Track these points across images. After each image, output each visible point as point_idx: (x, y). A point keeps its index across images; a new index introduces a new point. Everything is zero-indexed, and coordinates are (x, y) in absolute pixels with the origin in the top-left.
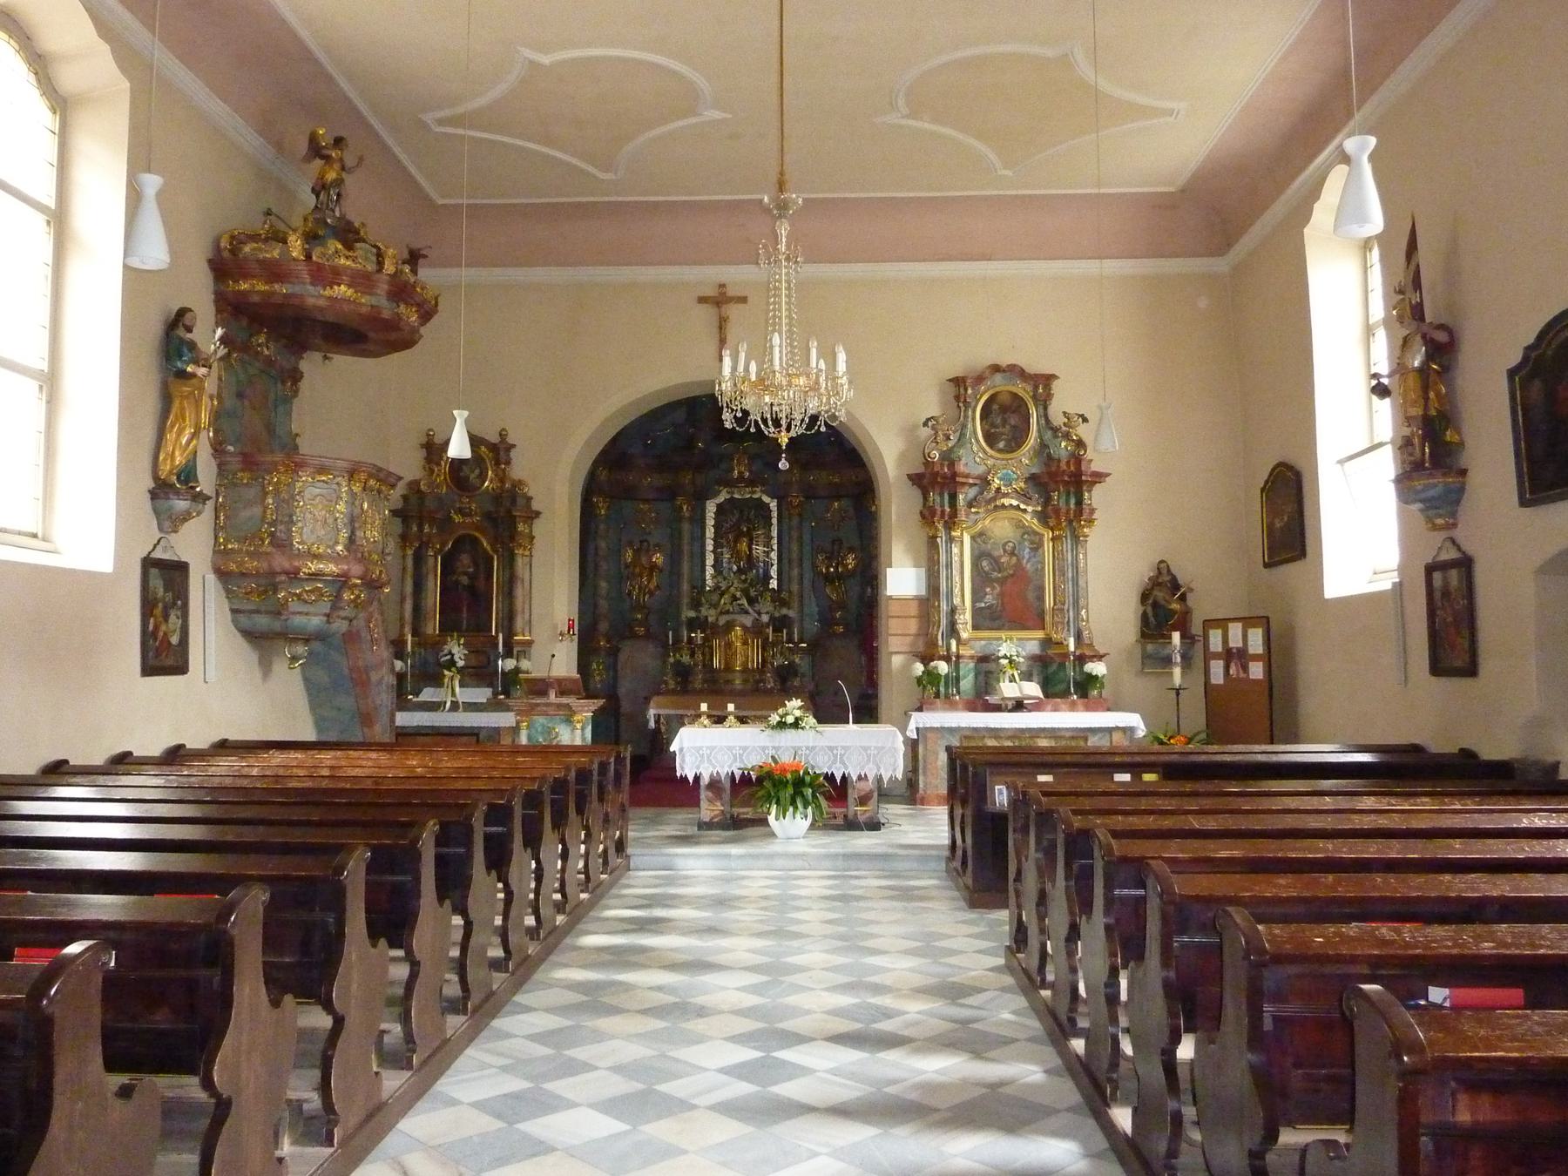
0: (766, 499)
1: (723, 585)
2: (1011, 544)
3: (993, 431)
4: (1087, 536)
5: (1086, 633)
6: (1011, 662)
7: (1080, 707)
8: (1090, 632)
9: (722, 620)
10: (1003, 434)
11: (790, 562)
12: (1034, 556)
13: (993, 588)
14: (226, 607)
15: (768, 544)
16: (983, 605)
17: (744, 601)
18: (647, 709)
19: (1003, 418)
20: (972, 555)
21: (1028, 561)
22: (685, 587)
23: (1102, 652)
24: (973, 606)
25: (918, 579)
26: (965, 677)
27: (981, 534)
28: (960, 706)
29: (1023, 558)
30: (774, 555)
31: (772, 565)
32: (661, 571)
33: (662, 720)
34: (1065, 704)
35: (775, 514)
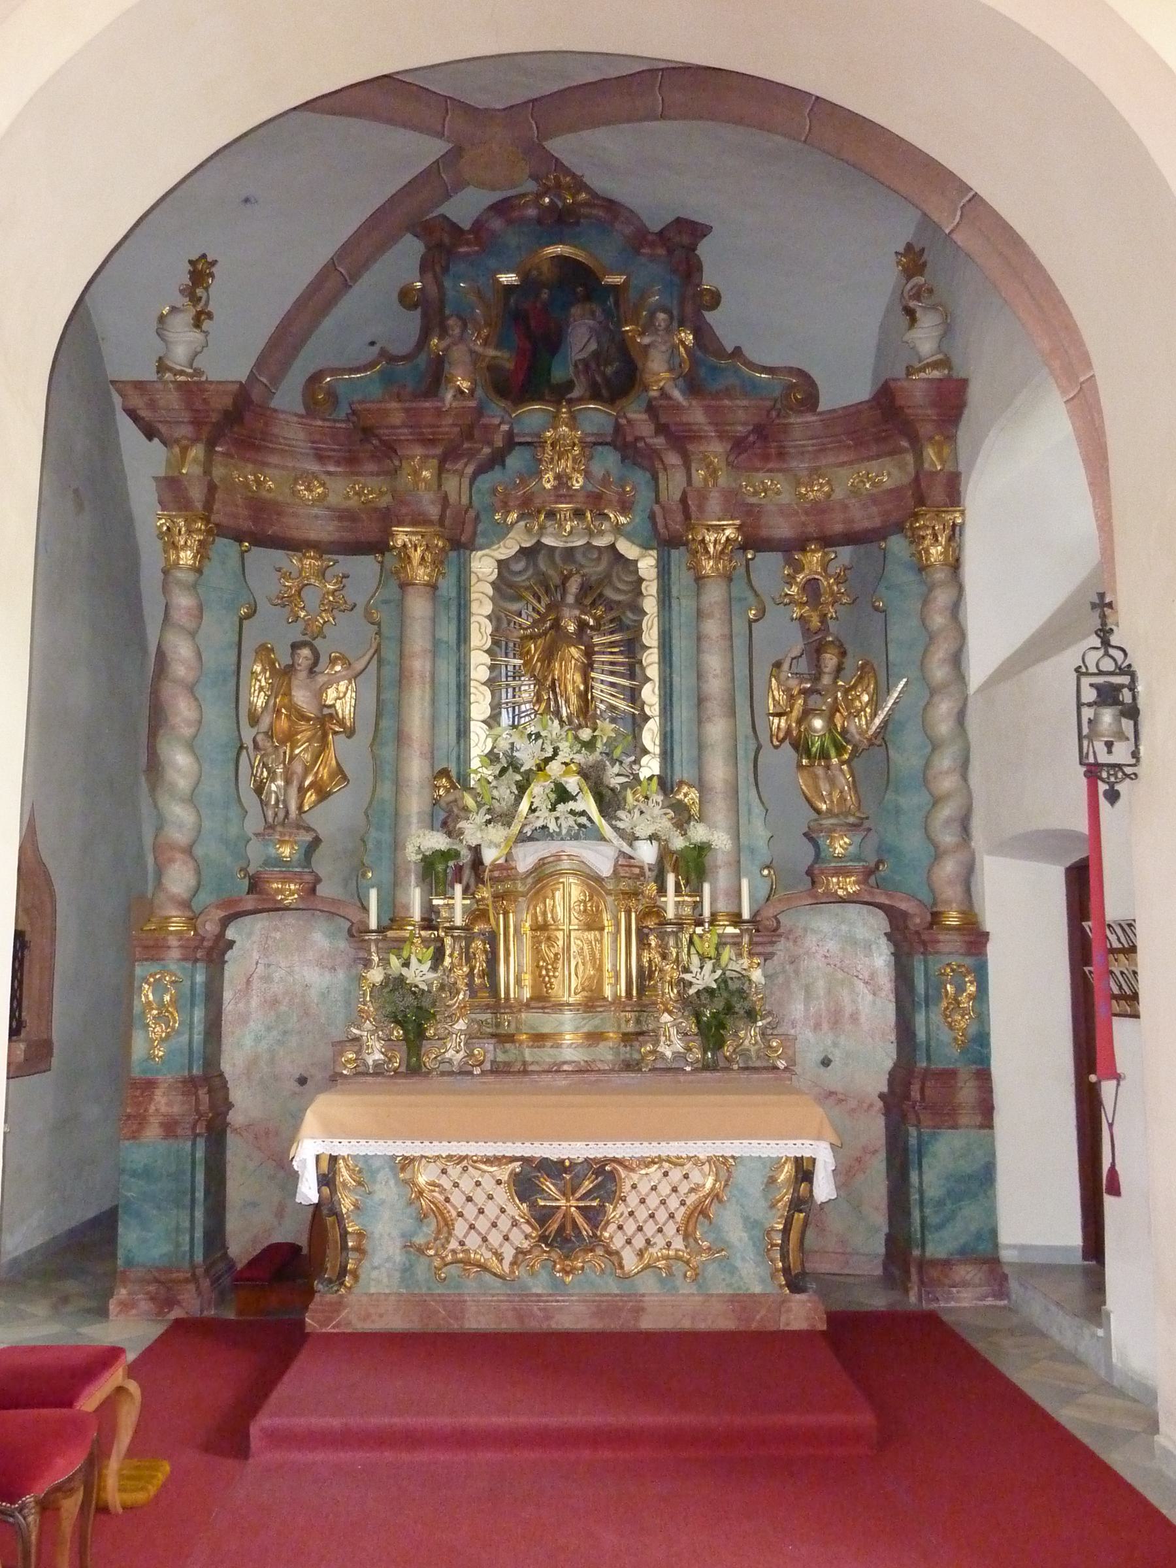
0: (628, 549)
1: (528, 756)
9: (526, 858)
11: (700, 701)
15: (634, 670)
17: (588, 804)
18: (292, 1138)
22: (416, 769)
24: (701, 897)
30: (650, 695)
31: (647, 718)
32: (350, 733)
33: (344, 1175)
35: (651, 589)
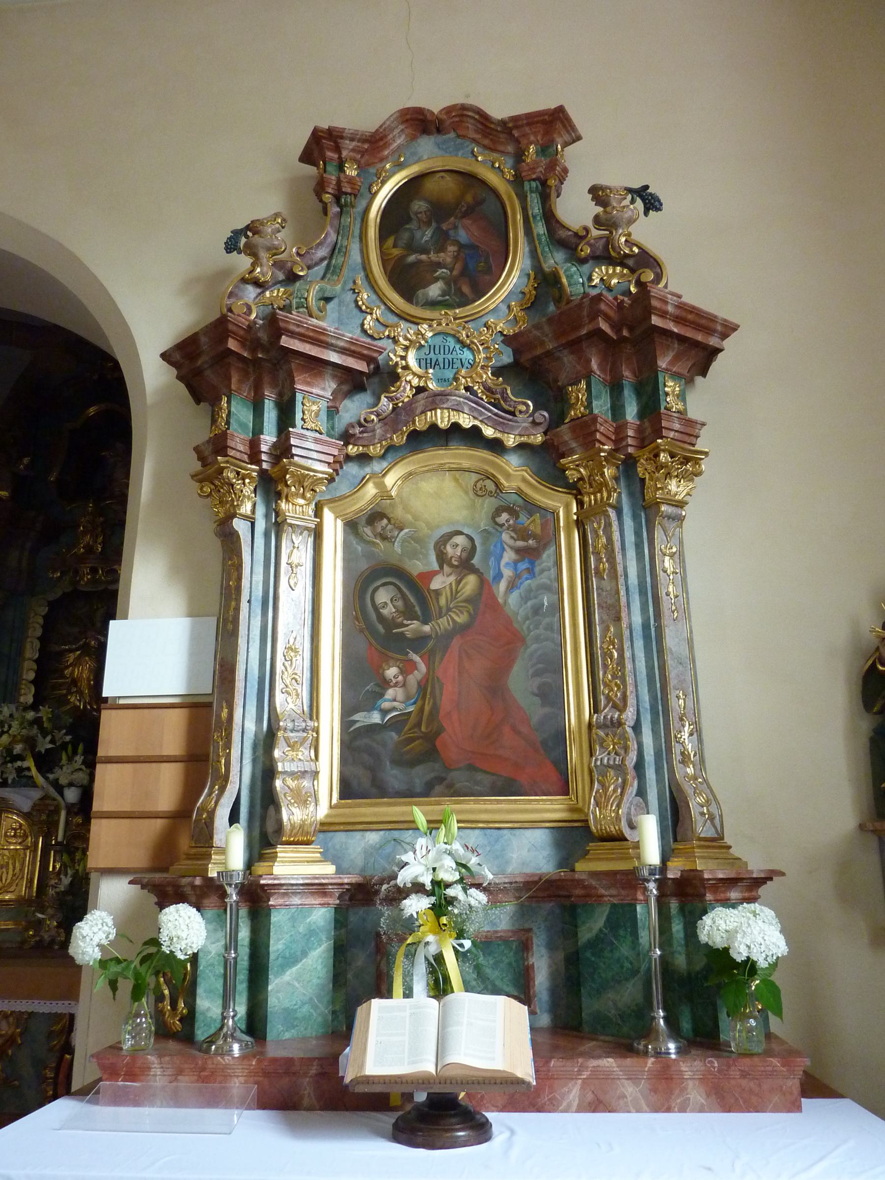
2: (460, 540)
3: (412, 258)
4: (681, 504)
5: (696, 803)
6: (444, 904)
7: (695, 1093)
8: (712, 799)
10: (439, 265)
12: (531, 571)
13: (407, 668)
14: (641, 850)
16: (376, 718)
17: (30, 763)
19: (438, 229)
20: (347, 570)
21: (512, 586)
23: (756, 866)
24: (346, 723)
25: (195, 640)
26: (291, 960)
27: (375, 516)
28: (237, 1085)
29: (499, 576)
34: (633, 1078)
